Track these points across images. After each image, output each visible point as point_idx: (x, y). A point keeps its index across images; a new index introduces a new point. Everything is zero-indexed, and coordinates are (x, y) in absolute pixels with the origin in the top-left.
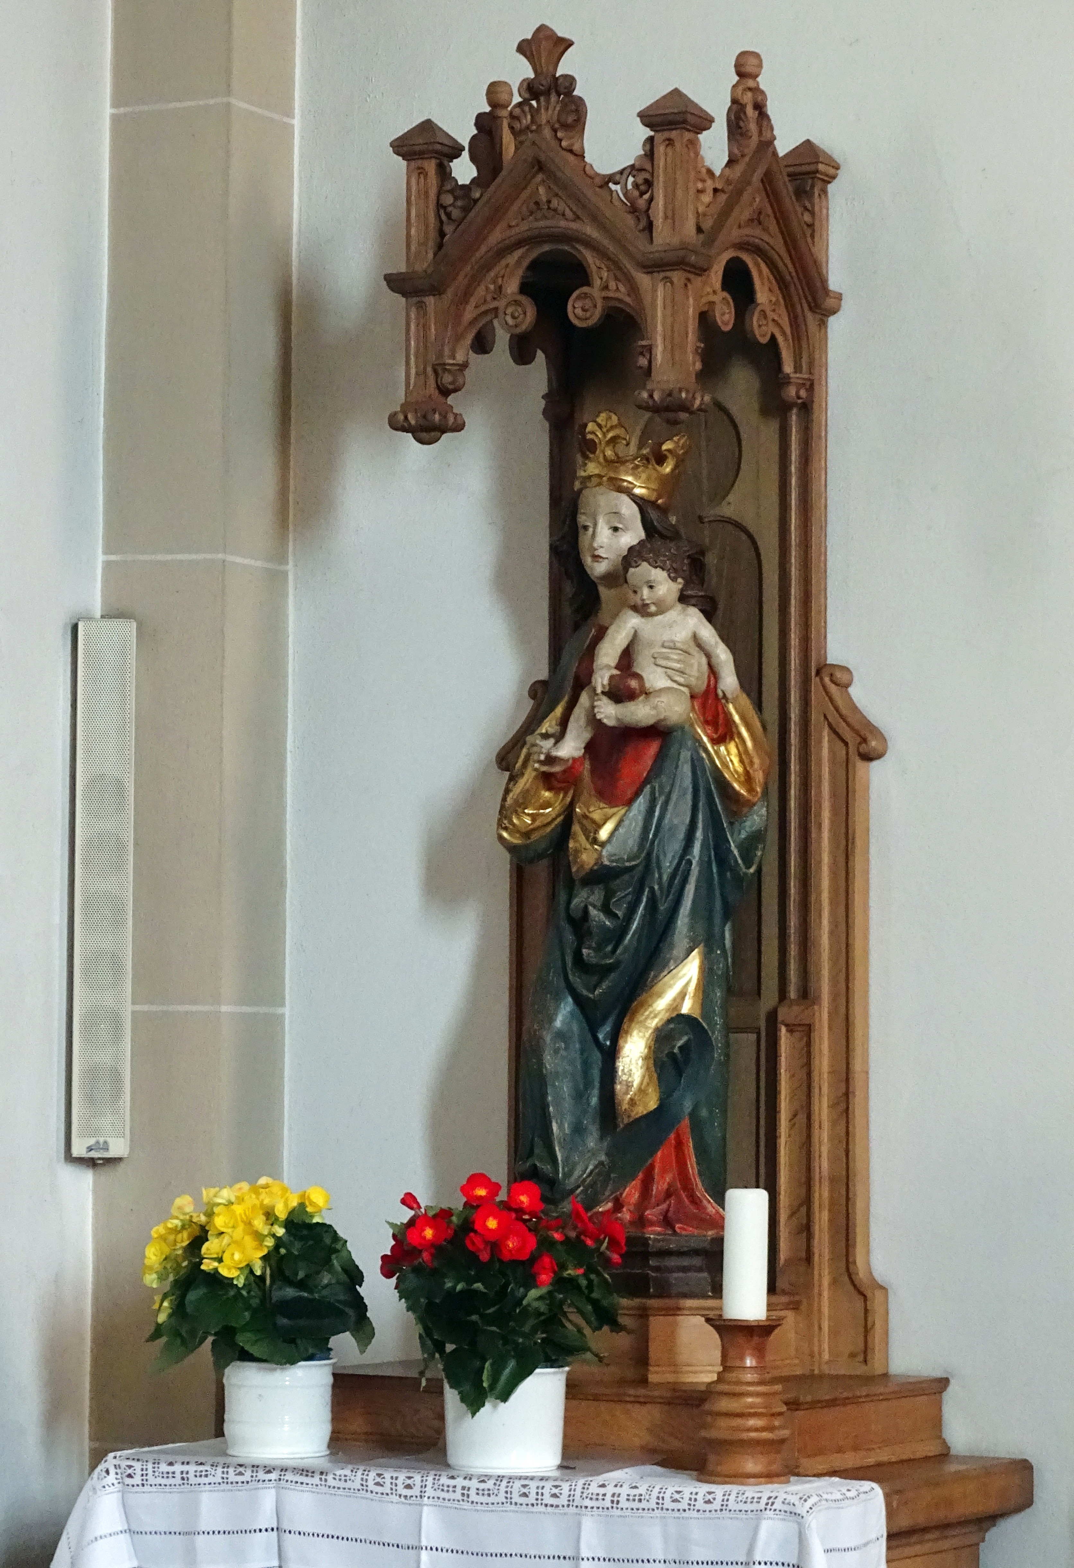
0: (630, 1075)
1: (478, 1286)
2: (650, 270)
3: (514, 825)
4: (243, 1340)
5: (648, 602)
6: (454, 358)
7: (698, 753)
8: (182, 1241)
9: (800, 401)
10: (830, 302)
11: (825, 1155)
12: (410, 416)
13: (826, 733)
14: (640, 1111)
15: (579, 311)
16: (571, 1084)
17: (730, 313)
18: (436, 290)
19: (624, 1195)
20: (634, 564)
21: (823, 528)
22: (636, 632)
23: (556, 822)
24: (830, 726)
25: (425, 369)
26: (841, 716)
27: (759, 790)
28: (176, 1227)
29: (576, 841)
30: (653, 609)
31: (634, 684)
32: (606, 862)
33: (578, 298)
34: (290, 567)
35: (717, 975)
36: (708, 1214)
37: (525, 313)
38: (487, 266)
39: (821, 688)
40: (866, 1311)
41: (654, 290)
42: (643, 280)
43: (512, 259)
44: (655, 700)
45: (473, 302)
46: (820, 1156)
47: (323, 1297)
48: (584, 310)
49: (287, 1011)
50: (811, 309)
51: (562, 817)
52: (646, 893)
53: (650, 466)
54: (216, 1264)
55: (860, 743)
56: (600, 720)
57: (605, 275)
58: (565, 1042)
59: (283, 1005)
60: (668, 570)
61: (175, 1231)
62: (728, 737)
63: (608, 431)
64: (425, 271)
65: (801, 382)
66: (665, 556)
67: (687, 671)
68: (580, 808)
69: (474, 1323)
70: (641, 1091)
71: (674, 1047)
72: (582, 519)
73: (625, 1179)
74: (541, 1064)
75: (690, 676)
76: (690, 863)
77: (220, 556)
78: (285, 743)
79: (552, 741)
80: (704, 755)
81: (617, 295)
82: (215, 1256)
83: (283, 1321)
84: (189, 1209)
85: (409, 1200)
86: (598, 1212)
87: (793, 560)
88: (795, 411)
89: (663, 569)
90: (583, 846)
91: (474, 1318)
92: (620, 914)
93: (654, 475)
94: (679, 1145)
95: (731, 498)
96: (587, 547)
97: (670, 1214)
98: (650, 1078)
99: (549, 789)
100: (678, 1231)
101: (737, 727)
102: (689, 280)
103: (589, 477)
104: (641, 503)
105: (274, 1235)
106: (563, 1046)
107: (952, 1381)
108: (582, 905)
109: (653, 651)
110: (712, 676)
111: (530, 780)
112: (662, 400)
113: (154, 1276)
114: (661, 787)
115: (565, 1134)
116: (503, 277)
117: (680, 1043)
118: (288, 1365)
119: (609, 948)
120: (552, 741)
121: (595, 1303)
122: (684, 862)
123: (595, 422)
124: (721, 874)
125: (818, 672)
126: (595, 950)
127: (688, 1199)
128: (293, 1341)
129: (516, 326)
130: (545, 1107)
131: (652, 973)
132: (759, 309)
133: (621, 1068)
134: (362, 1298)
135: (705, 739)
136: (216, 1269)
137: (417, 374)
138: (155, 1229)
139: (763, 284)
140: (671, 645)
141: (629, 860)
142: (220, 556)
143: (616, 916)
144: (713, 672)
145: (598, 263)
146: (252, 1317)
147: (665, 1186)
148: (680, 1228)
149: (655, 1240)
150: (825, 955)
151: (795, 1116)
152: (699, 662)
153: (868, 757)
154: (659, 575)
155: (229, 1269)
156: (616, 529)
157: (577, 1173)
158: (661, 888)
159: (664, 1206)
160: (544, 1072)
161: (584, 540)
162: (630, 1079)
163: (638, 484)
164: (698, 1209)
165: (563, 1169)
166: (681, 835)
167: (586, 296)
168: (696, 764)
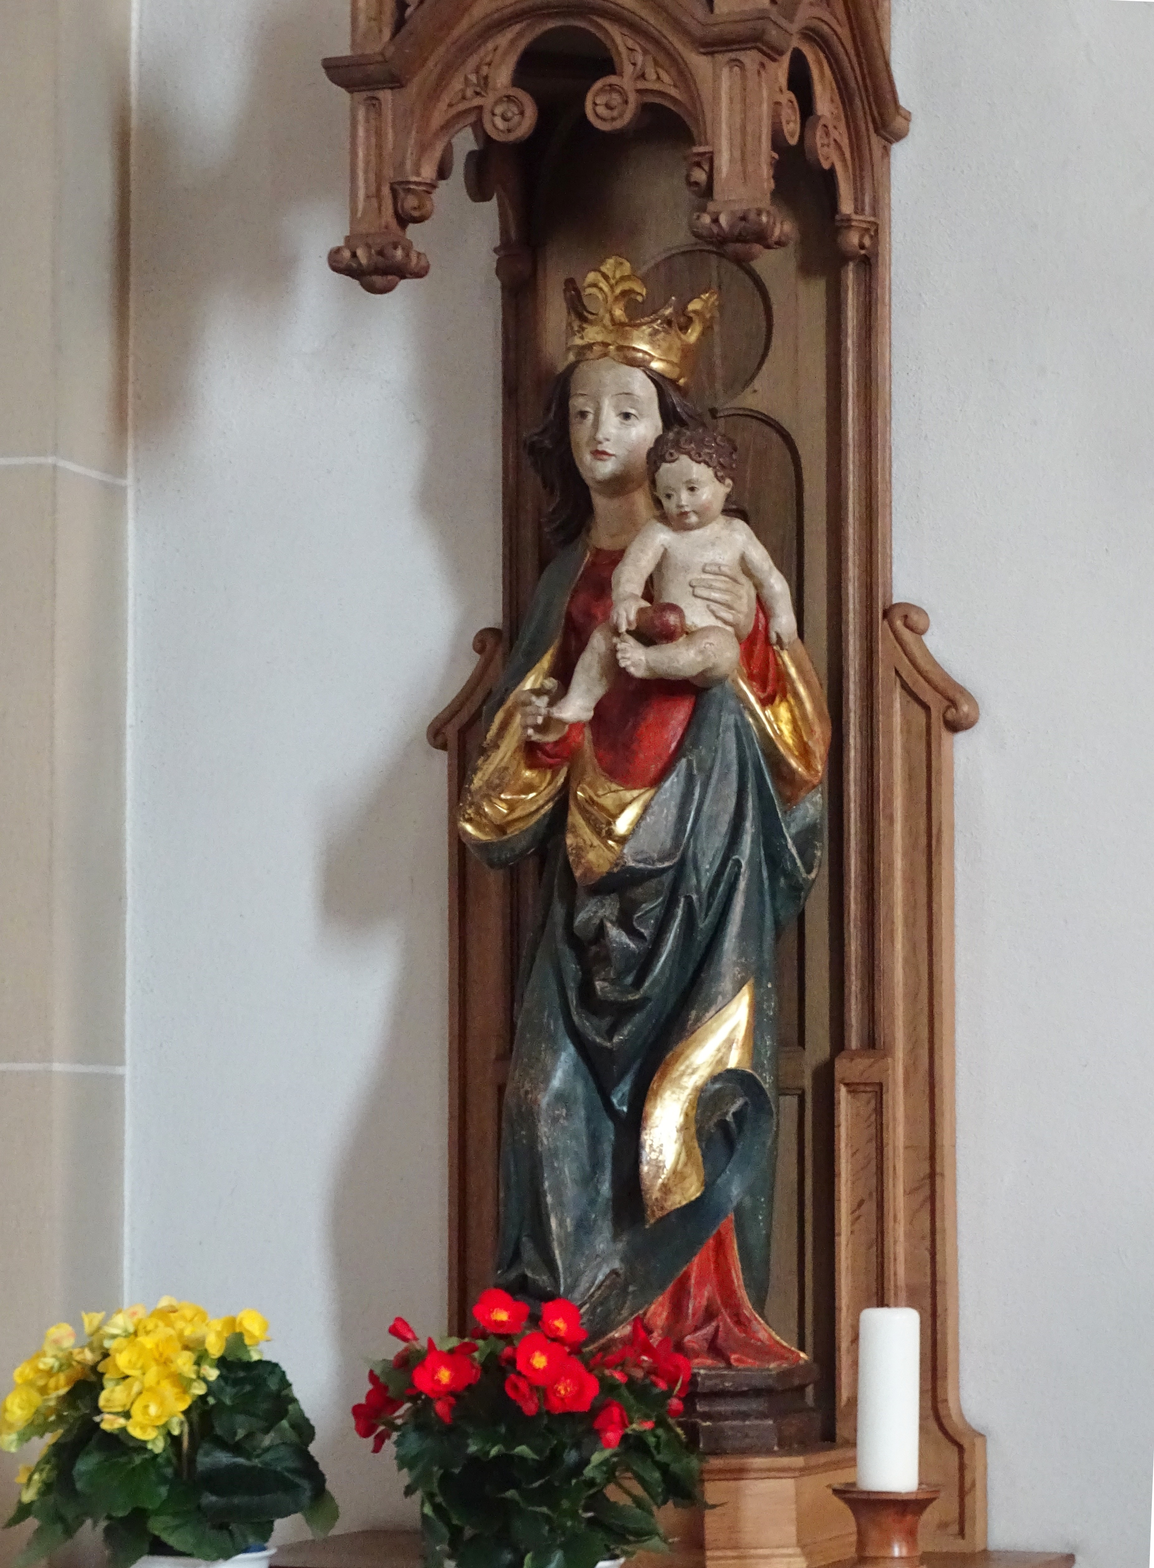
0: (661, 1152)
1: (522, 1449)
2: (710, 49)
3: (486, 815)
4: (157, 1526)
5: (687, 509)
6: (418, 174)
7: (742, 717)
8: (57, 1388)
9: (863, 252)
10: (899, 122)
11: (901, 1258)
12: (360, 252)
13: (898, 695)
14: (678, 1200)
15: (601, 110)
16: (575, 1166)
17: (795, 122)
18: (396, 82)
19: (648, 1315)
20: (668, 457)
21: (887, 422)
22: (666, 550)
23: (543, 812)
24: (905, 686)
25: (379, 190)
26: (920, 672)
27: (820, 768)
28: (52, 1368)
29: (576, 835)
30: (693, 519)
31: (672, 619)
32: (631, 864)
33: (602, 90)
34: (129, 481)
35: (767, 1015)
36: (759, 1340)
37: (522, 113)
38: (467, 48)
39: (892, 636)
40: (962, 1467)
41: (716, 78)
42: (699, 63)
43: (503, 39)
44: (703, 643)
45: (446, 99)
46: (895, 1260)
47: (266, 1464)
48: (608, 106)
49: (127, 1071)
50: (876, 131)
51: (551, 805)
52: (681, 905)
53: (673, 332)
54: (121, 1421)
55: (948, 708)
56: (624, 669)
57: (639, 58)
58: (568, 1109)
59: (122, 1063)
60: (714, 468)
61: (50, 1373)
62: (777, 699)
63: (617, 283)
64: (382, 54)
65: (864, 225)
66: (711, 447)
67: (735, 606)
68: (583, 791)
69: (512, 1501)
70: (677, 1174)
71: (726, 1113)
72: (577, 403)
73: (647, 1292)
74: (534, 1138)
75: (739, 612)
76: (738, 863)
77: (50, 460)
78: (124, 714)
79: (545, 699)
80: (751, 720)
81: (656, 86)
82: (120, 1409)
83: (209, 1499)
84: (68, 1343)
85: (399, 1329)
86: (613, 1340)
87: (851, 467)
88: (851, 266)
89: (709, 466)
90: (588, 843)
91: (511, 1493)
92: (646, 932)
93: (678, 343)
94: (720, 1246)
95: (757, 384)
96: (586, 439)
97: (720, 1341)
98: (689, 1154)
99: (531, 767)
100: (735, 1364)
101: (792, 682)
102: (762, 65)
103: (590, 346)
104: (658, 380)
105: (204, 1380)
106: (564, 1112)
107: (1078, 1558)
108: (596, 921)
109: (689, 577)
110: (761, 615)
111: (509, 754)
112: (732, 226)
113: (14, 1436)
114: (700, 761)
115: (566, 1233)
116: (489, 64)
117: (734, 1109)
118: (221, 1561)
119: (629, 980)
120: (545, 699)
121: (664, 1469)
122: (731, 862)
123: (600, 271)
124: (773, 879)
125: (886, 614)
126: (613, 982)
127: (731, 1318)
128: (223, 1527)
129: (509, 131)
130: (537, 1196)
131: (693, 1014)
132: (822, 122)
133: (648, 1143)
134: (316, 1464)
135: (752, 699)
136: (124, 1430)
137: (368, 197)
138: (17, 1372)
139: (824, 89)
140: (715, 569)
141: (662, 860)
142: (50, 460)
143: (641, 936)
144: (763, 606)
145: (630, 43)
146: (170, 1491)
147: (704, 1302)
148: (738, 1360)
149: (706, 1377)
150: (899, 991)
151: (861, 1204)
152: (747, 592)
153: (954, 727)
154: (701, 472)
155: (143, 1428)
156: (627, 416)
157: (584, 1284)
158: (699, 899)
159: (708, 1330)
160: (540, 1149)
161: (581, 432)
162: (661, 1158)
163: (657, 356)
164: (745, 1332)
165: (565, 1280)
166: (724, 827)
167: (612, 88)
168: (741, 731)
